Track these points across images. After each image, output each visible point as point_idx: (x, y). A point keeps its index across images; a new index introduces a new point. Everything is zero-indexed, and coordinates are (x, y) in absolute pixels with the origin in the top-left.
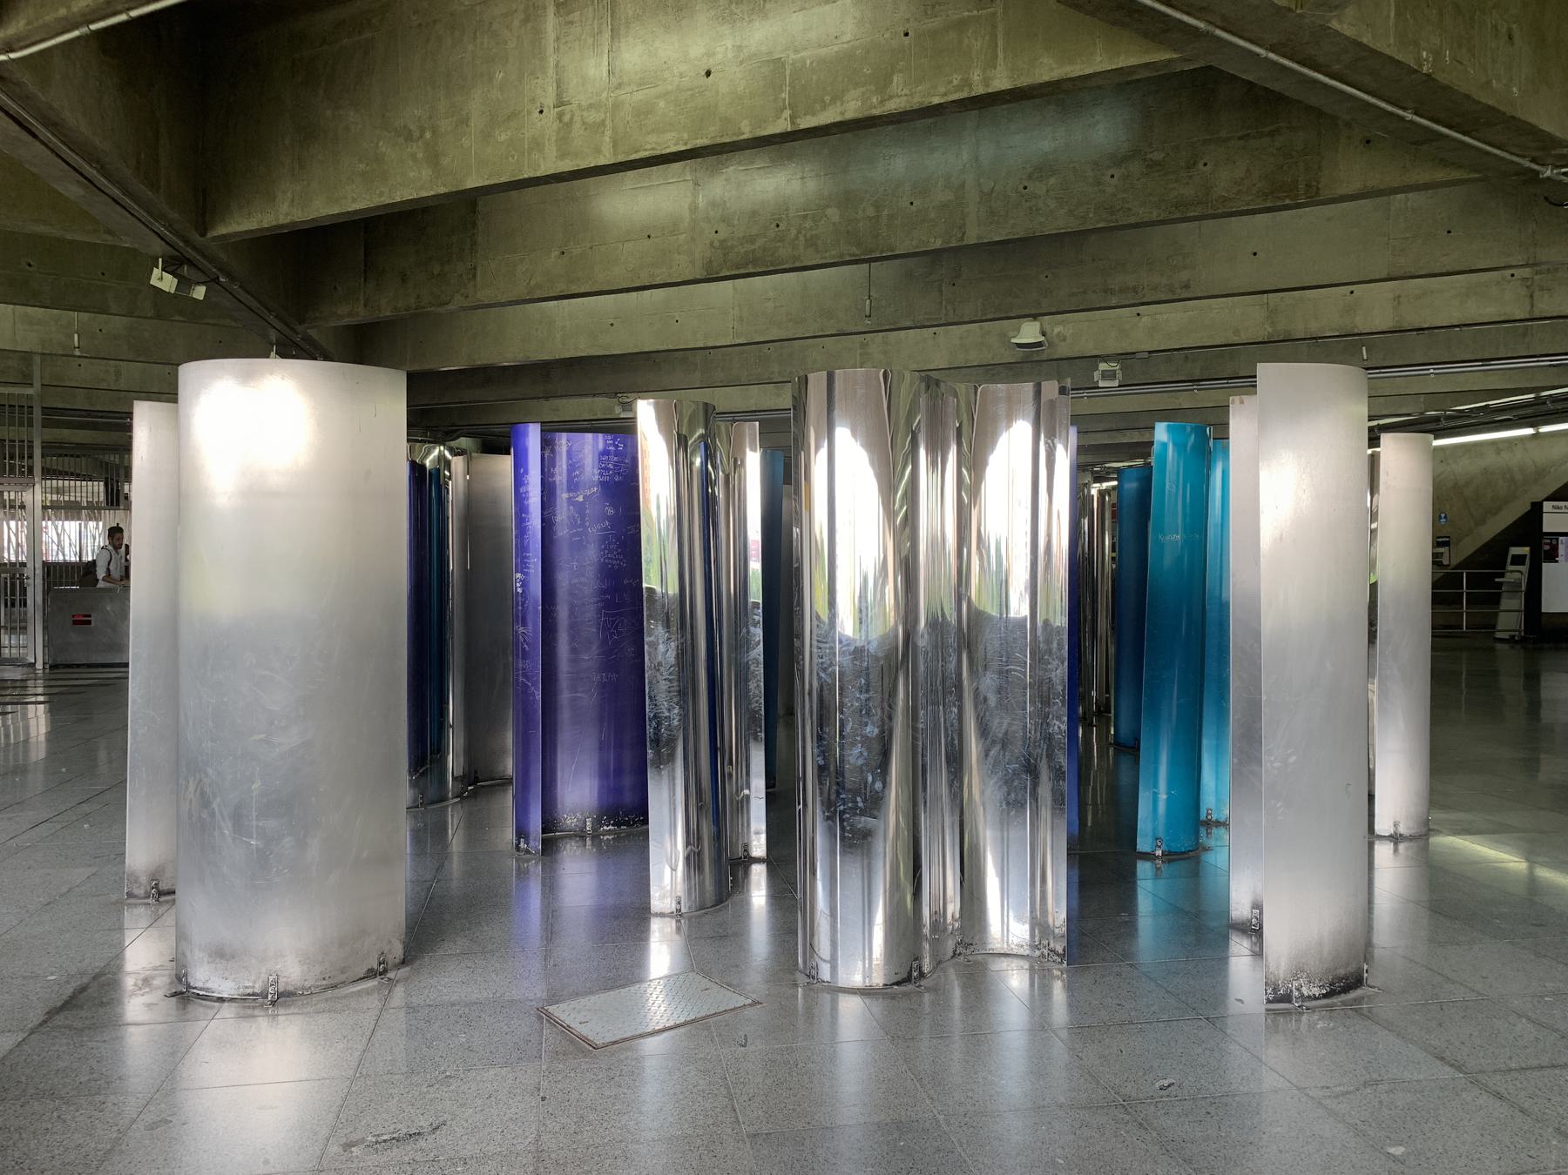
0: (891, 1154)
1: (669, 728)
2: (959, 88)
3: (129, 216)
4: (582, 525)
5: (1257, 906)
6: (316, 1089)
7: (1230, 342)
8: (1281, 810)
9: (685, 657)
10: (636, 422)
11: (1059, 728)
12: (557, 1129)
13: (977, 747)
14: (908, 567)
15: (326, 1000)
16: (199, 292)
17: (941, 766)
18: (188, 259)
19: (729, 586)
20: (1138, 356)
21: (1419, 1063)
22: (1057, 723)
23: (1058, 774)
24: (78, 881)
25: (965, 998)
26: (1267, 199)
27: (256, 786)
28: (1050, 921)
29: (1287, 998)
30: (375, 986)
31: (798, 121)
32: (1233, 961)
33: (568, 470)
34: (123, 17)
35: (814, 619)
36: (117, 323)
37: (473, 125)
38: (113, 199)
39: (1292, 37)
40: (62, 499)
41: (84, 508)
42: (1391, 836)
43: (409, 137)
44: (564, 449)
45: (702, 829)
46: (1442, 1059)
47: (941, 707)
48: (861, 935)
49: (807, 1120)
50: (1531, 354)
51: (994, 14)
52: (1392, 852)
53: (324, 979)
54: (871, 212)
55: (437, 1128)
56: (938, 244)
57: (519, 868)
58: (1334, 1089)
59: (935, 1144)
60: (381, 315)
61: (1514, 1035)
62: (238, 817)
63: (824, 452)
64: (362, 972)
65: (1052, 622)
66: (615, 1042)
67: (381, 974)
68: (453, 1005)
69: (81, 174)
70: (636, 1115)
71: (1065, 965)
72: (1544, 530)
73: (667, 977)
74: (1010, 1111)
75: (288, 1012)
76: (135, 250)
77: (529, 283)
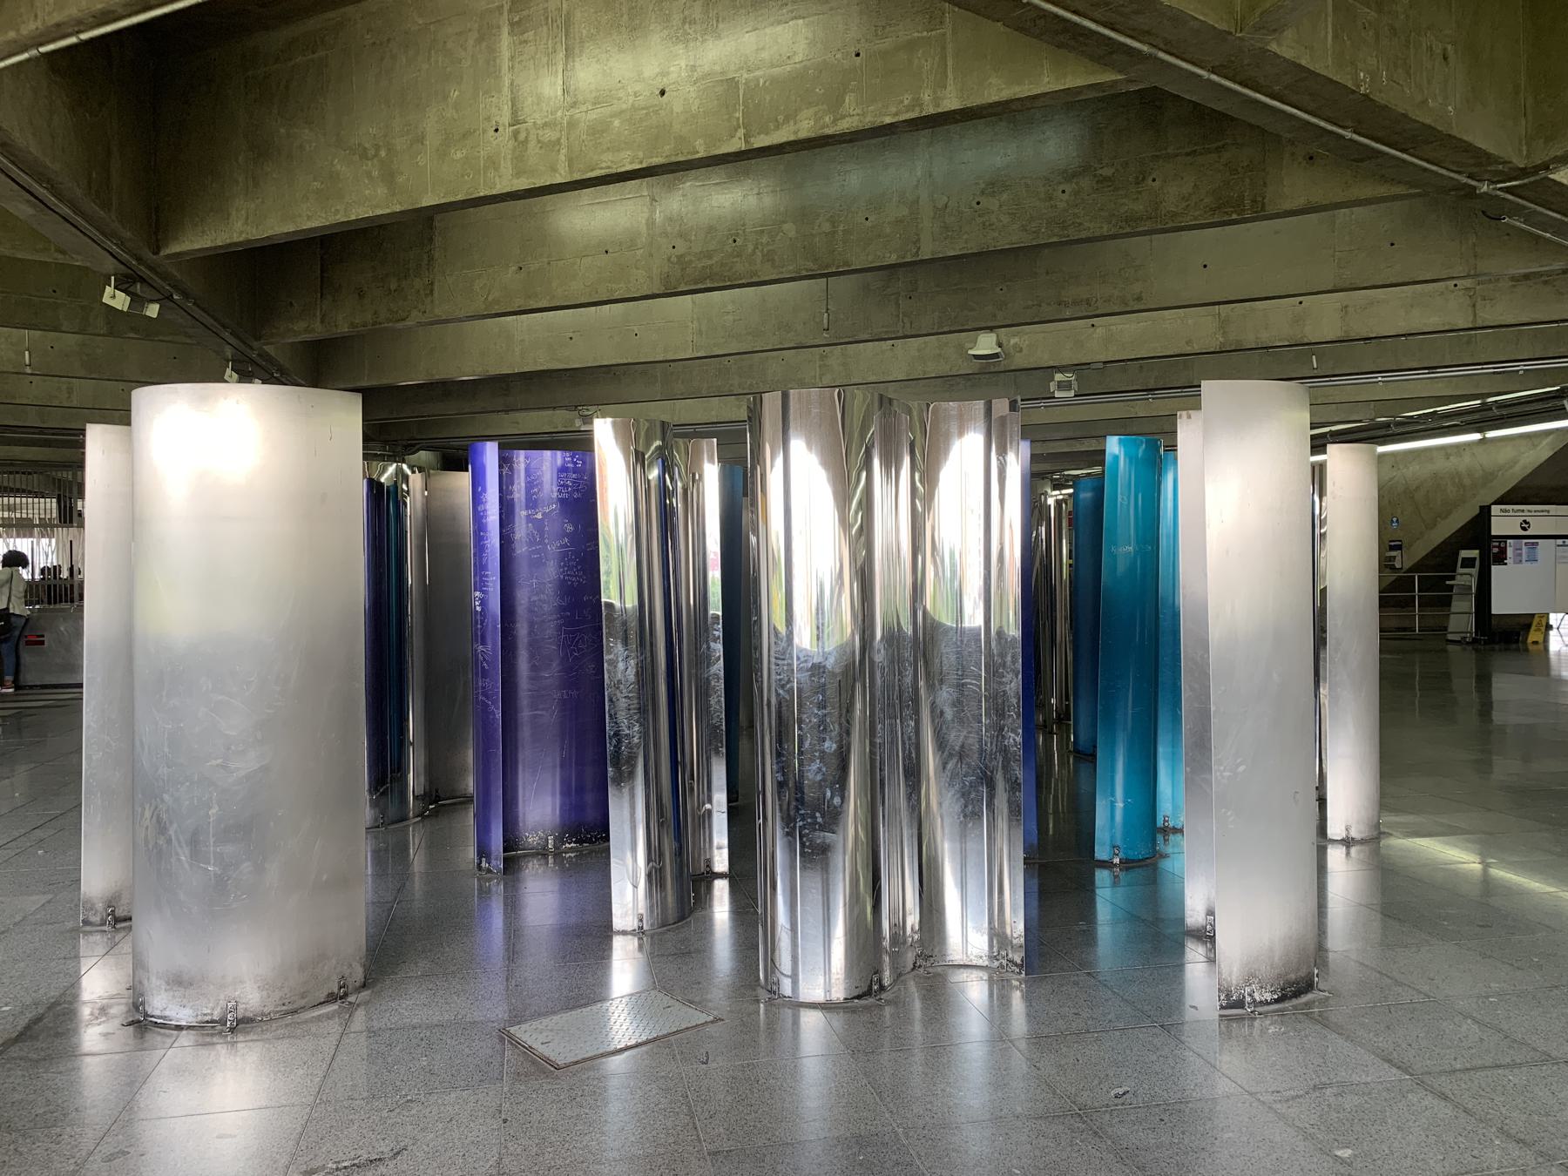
0: (851, 1168)
1: (629, 746)
2: (909, 108)
3: (79, 233)
4: (542, 542)
5: (1211, 912)
6: (276, 1116)
8: (1231, 819)
9: (645, 674)
10: (593, 435)
11: (1014, 740)
12: (519, 1151)
13: (934, 761)
14: (864, 577)
15: (287, 1025)
16: (153, 310)
17: (899, 784)
18: (141, 277)
19: (689, 598)
20: (1093, 366)
21: (1367, 1066)
22: (1013, 735)
23: (1014, 786)
24: (33, 909)
25: (925, 1009)
26: (1214, 214)
27: (213, 811)
28: (1008, 931)
29: (1240, 1004)
30: (335, 1010)
31: (752, 140)
32: (1189, 967)
33: (526, 487)
34: (73, 40)
35: (772, 636)
36: (70, 340)
37: (428, 143)
38: (64, 218)
39: (1233, 58)
40: (13, 516)
41: (37, 526)
42: (1343, 840)
43: (364, 156)
44: (522, 466)
45: (664, 845)
46: (1389, 1061)
47: (898, 721)
48: (822, 949)
49: (768, 1137)
50: (1475, 362)
51: (944, 35)
52: (1344, 856)
53: (284, 1005)
54: (827, 227)
55: (398, 1153)
56: (893, 259)
57: (480, 887)
58: (1284, 1093)
59: (894, 1157)
60: (339, 331)
61: (1459, 1036)
62: (194, 842)
63: (779, 460)
64: (322, 996)
65: (1006, 631)
66: (577, 1063)
67: (341, 998)
68: (415, 1028)
69: (32, 194)
70: (598, 1136)
71: (1023, 975)
72: (1493, 533)
73: (628, 995)
74: (968, 1122)
75: (248, 1038)
76: (87, 268)
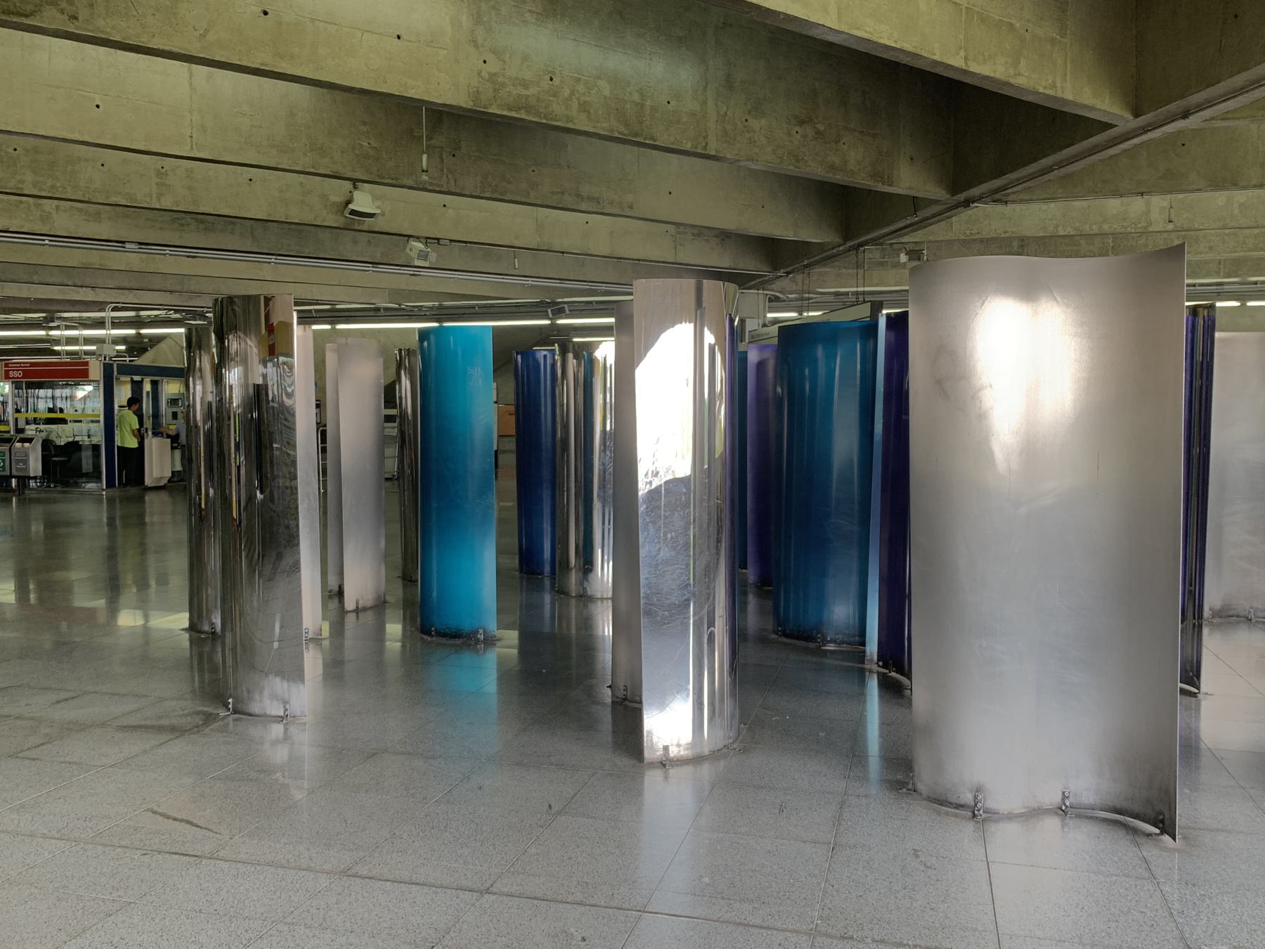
54: (636, 98)
77: (203, 36)
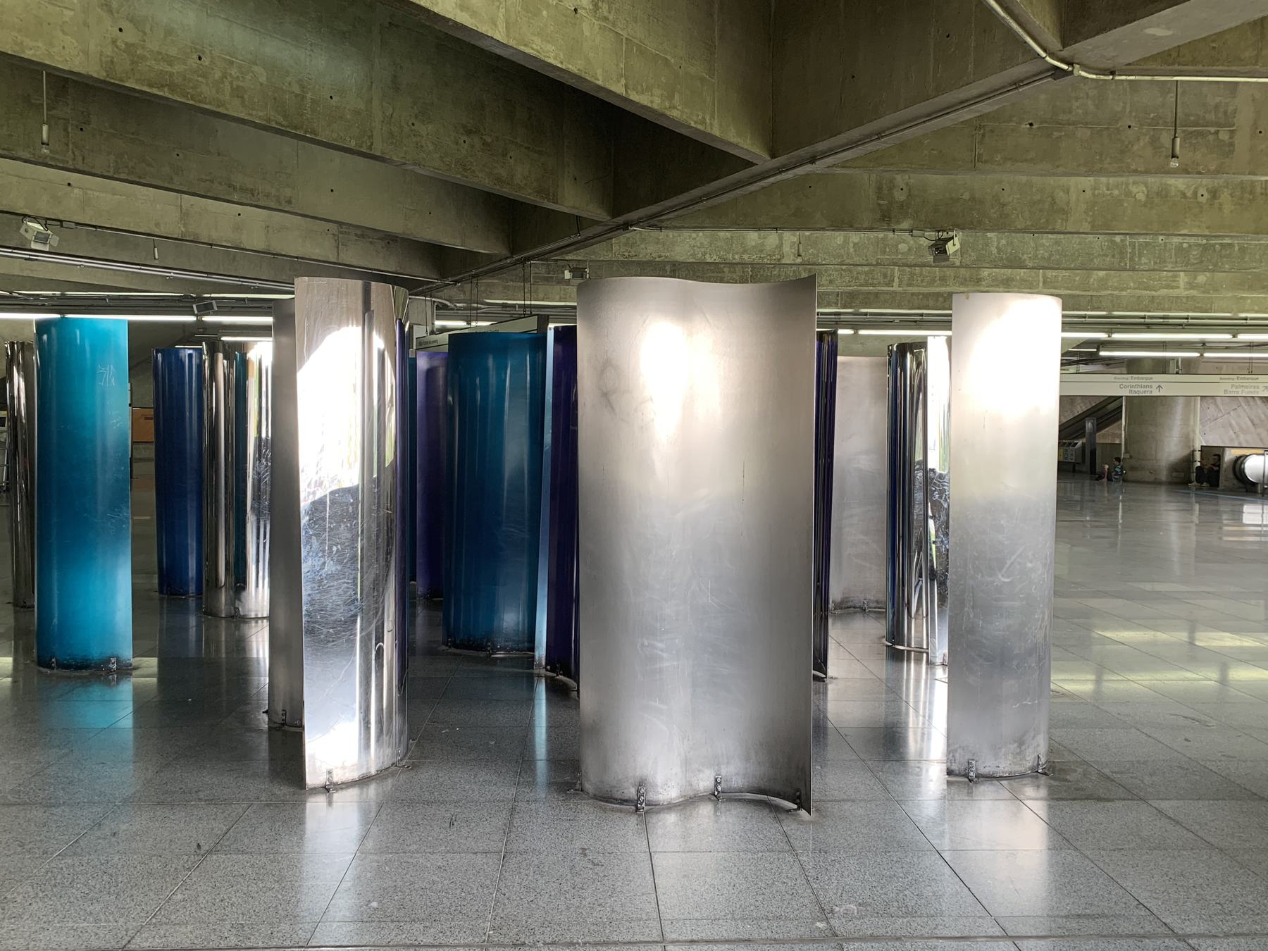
7: (152, 233)
50: (132, 261)
